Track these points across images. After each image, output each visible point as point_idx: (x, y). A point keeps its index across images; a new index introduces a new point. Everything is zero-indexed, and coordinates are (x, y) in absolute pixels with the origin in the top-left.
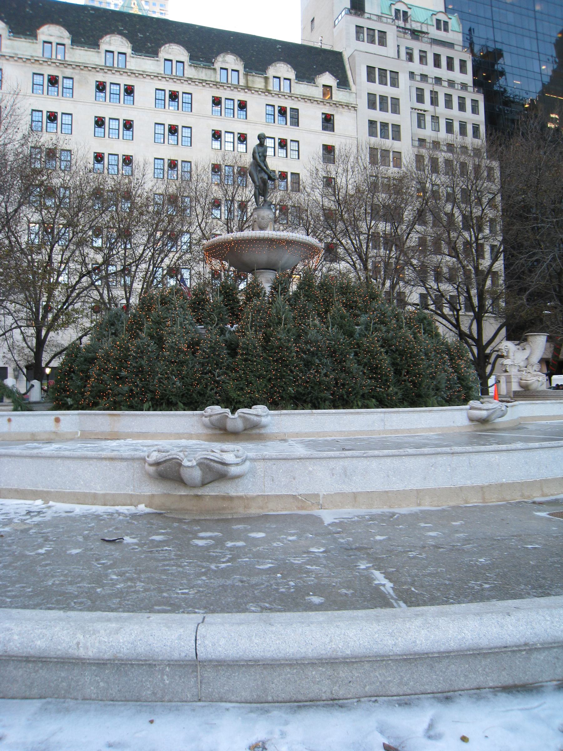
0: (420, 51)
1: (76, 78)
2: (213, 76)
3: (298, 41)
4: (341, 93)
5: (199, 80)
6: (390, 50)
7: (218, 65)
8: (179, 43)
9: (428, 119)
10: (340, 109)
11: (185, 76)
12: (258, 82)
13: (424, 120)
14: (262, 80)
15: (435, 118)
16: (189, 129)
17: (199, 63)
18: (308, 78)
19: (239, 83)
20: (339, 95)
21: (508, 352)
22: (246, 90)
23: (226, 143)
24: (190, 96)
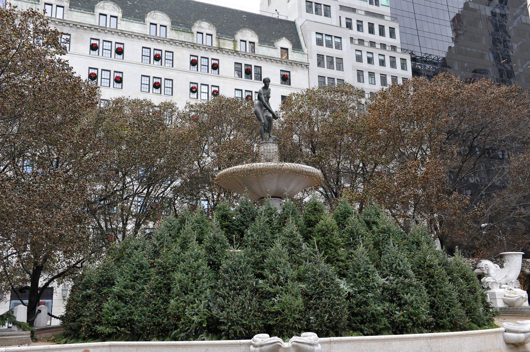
0: (357, 21)
1: (73, 35)
2: (191, 38)
3: (258, 12)
4: (296, 54)
5: (180, 41)
6: (334, 20)
7: (195, 30)
8: (162, 10)
9: (366, 75)
10: (295, 67)
11: (168, 37)
12: (228, 45)
13: (363, 76)
14: (232, 43)
15: (371, 74)
16: (171, 81)
17: (179, 27)
18: (268, 42)
19: (212, 45)
20: (293, 56)
21: (488, 270)
22: (218, 51)
23: (202, 93)
24: (171, 54)
